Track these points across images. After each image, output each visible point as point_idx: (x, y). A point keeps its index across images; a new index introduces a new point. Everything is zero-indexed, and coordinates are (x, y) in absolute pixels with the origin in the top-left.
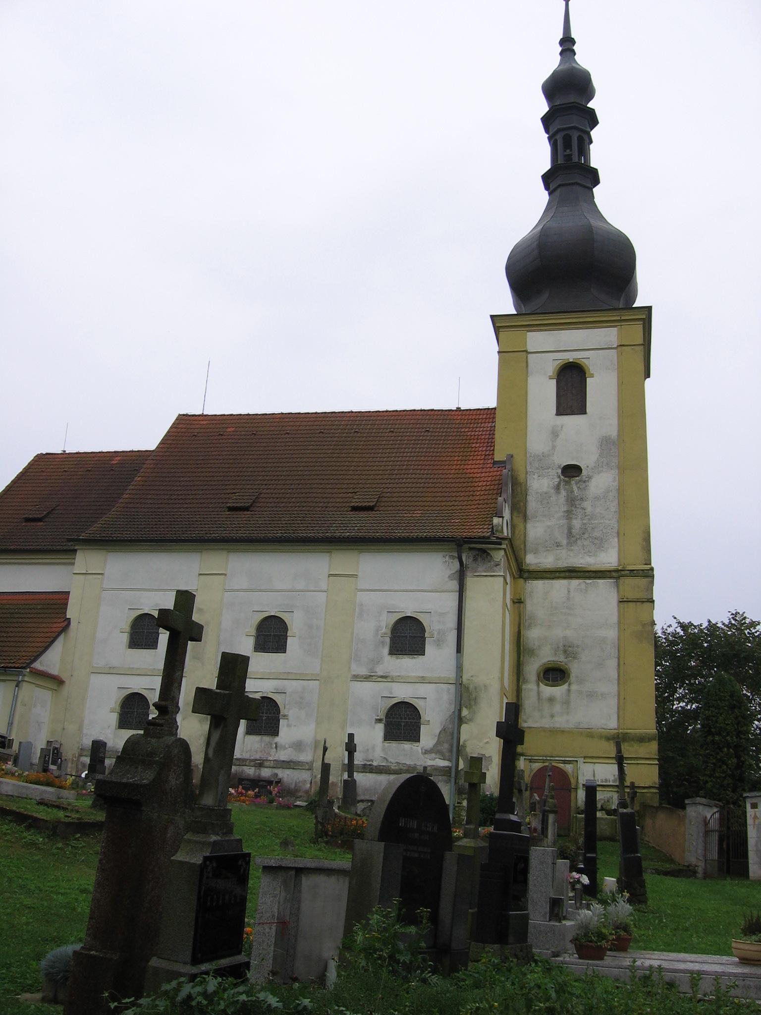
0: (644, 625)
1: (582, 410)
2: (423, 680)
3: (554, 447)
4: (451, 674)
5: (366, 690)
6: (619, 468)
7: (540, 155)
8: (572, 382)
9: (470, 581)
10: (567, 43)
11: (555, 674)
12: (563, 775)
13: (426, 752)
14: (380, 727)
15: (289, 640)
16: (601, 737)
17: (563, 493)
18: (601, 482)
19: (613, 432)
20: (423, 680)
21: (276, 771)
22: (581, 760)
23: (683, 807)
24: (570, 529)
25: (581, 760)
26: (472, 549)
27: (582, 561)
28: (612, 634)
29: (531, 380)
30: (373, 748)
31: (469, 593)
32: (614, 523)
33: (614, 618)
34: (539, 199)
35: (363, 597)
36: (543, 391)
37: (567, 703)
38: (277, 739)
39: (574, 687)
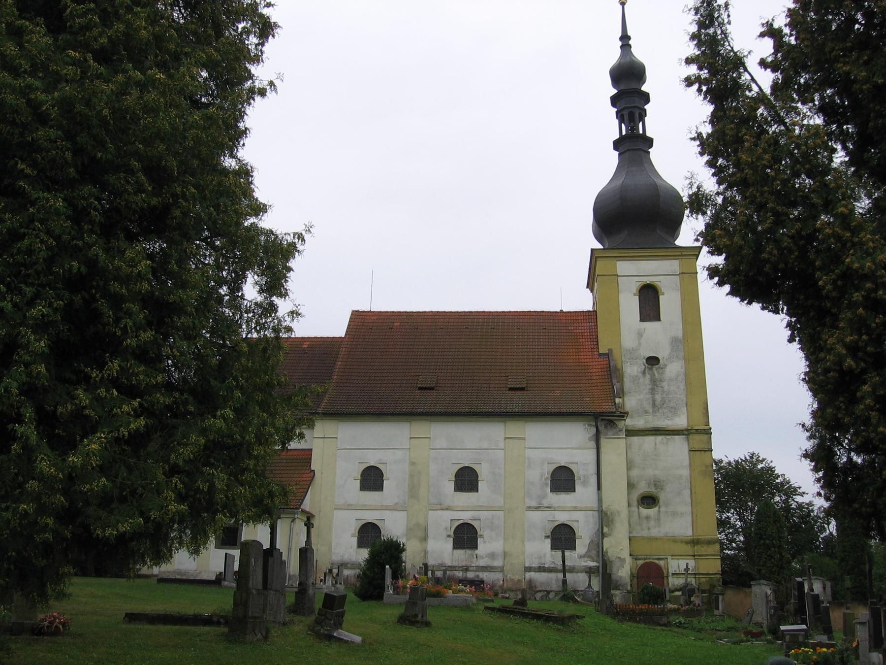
0: (707, 467)
1: (657, 318)
2: (575, 509)
3: (640, 344)
4: (595, 505)
5: (537, 517)
6: (685, 359)
7: (610, 127)
8: (649, 297)
9: (604, 442)
10: (625, 38)
11: (649, 500)
12: (659, 568)
13: (581, 557)
14: (548, 541)
15: (480, 483)
16: (682, 542)
17: (648, 376)
18: (673, 369)
19: (680, 334)
20: (575, 509)
21: (477, 573)
22: (669, 558)
23: (750, 586)
24: (654, 401)
25: (669, 558)
26: (605, 419)
27: (663, 423)
28: (685, 472)
29: (621, 296)
30: (545, 555)
31: (603, 450)
32: (683, 397)
33: (687, 462)
34: (613, 158)
35: (528, 453)
36: (630, 304)
37: (658, 520)
38: (477, 552)
39: (662, 509)
